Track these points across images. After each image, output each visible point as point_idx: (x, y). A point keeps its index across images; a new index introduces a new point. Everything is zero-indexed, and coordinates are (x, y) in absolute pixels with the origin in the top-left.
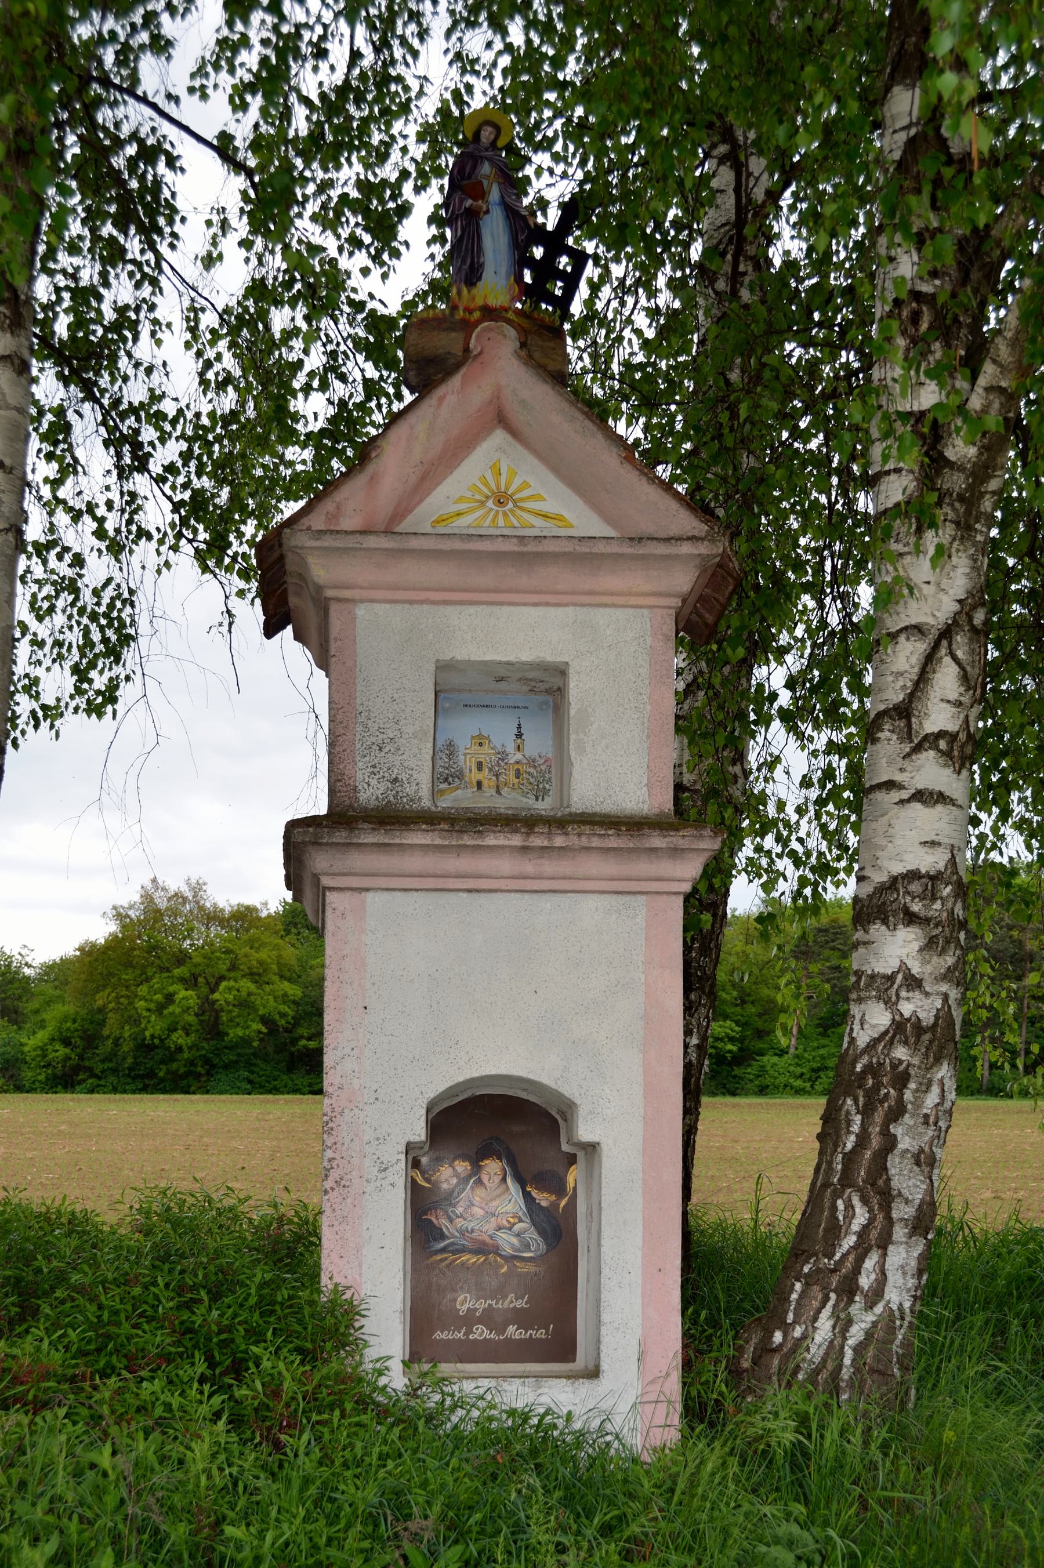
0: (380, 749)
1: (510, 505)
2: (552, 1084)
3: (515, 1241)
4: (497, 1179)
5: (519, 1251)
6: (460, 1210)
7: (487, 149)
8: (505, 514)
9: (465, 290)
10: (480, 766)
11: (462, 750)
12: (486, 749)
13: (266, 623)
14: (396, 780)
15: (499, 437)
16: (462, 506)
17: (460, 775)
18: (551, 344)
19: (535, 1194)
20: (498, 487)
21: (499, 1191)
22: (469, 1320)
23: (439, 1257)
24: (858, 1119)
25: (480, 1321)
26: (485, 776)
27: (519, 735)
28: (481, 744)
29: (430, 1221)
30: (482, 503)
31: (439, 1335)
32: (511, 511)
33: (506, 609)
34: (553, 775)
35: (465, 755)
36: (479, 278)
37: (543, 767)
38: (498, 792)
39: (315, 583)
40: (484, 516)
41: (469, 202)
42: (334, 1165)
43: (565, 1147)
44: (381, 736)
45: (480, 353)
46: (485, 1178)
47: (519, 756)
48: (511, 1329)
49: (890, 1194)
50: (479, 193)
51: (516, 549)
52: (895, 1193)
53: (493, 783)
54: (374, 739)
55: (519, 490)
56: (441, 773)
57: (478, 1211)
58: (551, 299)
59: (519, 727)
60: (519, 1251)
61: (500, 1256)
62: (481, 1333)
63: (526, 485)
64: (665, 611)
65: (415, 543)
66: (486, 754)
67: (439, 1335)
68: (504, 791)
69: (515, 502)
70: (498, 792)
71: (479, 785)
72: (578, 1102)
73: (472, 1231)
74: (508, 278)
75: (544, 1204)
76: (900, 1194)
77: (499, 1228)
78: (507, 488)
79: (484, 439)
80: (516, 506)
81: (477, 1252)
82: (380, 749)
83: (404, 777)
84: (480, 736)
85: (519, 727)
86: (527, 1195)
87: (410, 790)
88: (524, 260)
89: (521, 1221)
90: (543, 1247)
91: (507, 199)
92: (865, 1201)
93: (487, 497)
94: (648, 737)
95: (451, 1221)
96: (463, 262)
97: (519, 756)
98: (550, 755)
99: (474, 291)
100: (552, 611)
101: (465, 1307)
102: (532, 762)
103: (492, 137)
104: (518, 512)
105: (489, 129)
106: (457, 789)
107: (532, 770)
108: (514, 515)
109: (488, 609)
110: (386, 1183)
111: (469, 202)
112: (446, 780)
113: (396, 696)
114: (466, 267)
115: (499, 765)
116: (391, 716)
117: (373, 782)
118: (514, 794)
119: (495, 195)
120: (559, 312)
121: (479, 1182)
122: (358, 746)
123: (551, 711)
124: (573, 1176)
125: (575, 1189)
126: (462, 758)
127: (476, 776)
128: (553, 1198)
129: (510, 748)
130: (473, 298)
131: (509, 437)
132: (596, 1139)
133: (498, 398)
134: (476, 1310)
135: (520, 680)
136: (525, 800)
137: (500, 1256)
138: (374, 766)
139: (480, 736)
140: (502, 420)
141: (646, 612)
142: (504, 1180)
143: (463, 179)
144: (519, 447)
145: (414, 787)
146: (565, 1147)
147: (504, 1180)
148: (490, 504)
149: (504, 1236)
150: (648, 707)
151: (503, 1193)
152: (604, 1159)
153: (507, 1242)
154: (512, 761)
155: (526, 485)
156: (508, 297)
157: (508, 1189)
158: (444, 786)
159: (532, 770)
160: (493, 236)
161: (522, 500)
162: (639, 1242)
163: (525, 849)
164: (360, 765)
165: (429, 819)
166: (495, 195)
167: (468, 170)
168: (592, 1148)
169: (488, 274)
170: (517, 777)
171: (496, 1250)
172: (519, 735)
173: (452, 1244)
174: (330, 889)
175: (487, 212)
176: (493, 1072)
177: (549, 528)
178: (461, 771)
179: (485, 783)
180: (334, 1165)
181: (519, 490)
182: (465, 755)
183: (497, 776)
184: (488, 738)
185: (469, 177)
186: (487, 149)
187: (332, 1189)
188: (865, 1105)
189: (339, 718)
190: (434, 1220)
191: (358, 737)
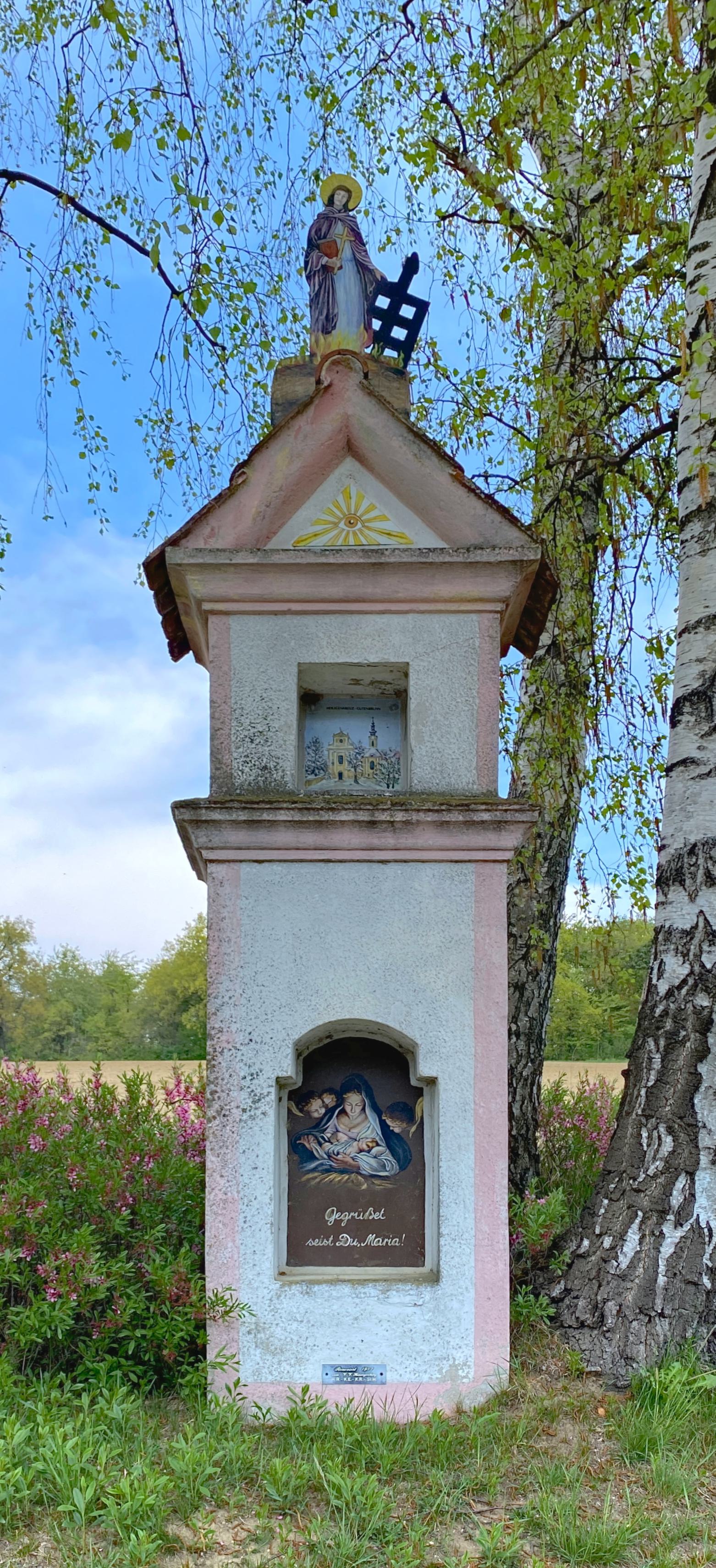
0: (252, 741)
1: (359, 525)
2: (398, 1028)
3: (373, 1162)
4: (358, 1109)
5: (376, 1170)
6: (327, 1135)
7: (340, 211)
8: (355, 533)
9: (321, 337)
10: (341, 760)
11: (326, 746)
12: (346, 745)
13: (170, 645)
14: (265, 768)
15: (349, 464)
16: (318, 528)
17: (324, 768)
18: (396, 384)
19: (389, 1122)
20: (349, 509)
21: (359, 1120)
22: (337, 1229)
23: (310, 1176)
24: (657, 1059)
25: (345, 1230)
26: (345, 767)
27: (373, 733)
28: (341, 741)
29: (304, 1146)
30: (336, 525)
31: (310, 1243)
32: (360, 530)
33: (356, 618)
34: (401, 767)
35: (328, 750)
36: (334, 327)
37: (393, 760)
38: (356, 781)
39: (195, 597)
40: (337, 536)
41: (325, 260)
42: (216, 1097)
43: (414, 1082)
44: (252, 730)
45: (329, 386)
46: (348, 1109)
47: (373, 751)
48: (371, 1237)
49: (697, 1126)
50: (333, 252)
51: (362, 561)
52: (700, 1124)
53: (352, 773)
54: (246, 733)
55: (367, 512)
56: (309, 767)
57: (342, 1137)
58: (395, 344)
59: (373, 726)
60: (376, 1170)
61: (361, 1174)
62: (346, 1240)
63: (372, 507)
64: (491, 615)
65: (276, 559)
66: (346, 750)
67: (310, 1243)
68: (361, 780)
69: (363, 522)
70: (356, 781)
71: (340, 775)
72: (419, 1042)
73: (338, 1154)
74: (358, 327)
75: (397, 1130)
76: (704, 1127)
77: (361, 1151)
78: (356, 510)
79: (337, 465)
80: (364, 526)
81: (342, 1172)
82: (252, 741)
83: (272, 765)
84: (341, 734)
85: (373, 726)
86: (384, 1126)
87: (277, 776)
88: (374, 312)
89: (378, 1145)
90: (396, 1167)
91: (358, 255)
92: (670, 1131)
93: (341, 519)
94: (477, 726)
95: (320, 1144)
96: (321, 313)
97: (373, 751)
98: (398, 749)
99: (330, 338)
100: (396, 619)
101: (332, 1219)
102: (384, 756)
103: (345, 200)
104: (367, 531)
105: (342, 193)
106: (322, 779)
107: (384, 762)
108: (362, 533)
109: (340, 618)
110: (258, 1112)
111: (325, 260)
112: (313, 772)
113: (264, 695)
114: (323, 317)
115: (357, 759)
116: (260, 712)
117: (247, 770)
118: (369, 783)
119: (346, 252)
120: (402, 355)
121: (343, 1112)
122: (233, 739)
123: (399, 710)
124: (423, 1106)
125: (422, 1118)
126: (326, 753)
127: (337, 768)
128: (404, 1125)
129: (366, 744)
130: (329, 345)
131: (357, 465)
132: (434, 1075)
133: (347, 427)
134: (341, 1221)
135: (372, 683)
136: (378, 788)
137: (361, 1174)
138: (247, 756)
139: (341, 734)
140: (351, 448)
141: (474, 617)
142: (364, 1109)
143: (319, 238)
144: (363, 470)
145: (280, 774)
146: (414, 1082)
147: (364, 1109)
148: (342, 525)
149: (364, 1158)
150: (477, 701)
151: (363, 1121)
152: (441, 1092)
153: (366, 1163)
154: (367, 755)
155: (372, 507)
156: (359, 343)
157: (366, 1117)
158: (312, 777)
159: (384, 762)
160: (345, 288)
161: (369, 520)
162: (471, 1163)
163: (372, 824)
164: (235, 755)
165: (293, 801)
166: (346, 252)
167: (323, 231)
168: (432, 1082)
169: (342, 322)
170: (372, 768)
171: (357, 1170)
172: (373, 733)
173: (322, 1164)
174: (212, 861)
175: (341, 268)
176: (347, 1017)
177: (393, 543)
178: (325, 765)
179: (345, 774)
180: (216, 1097)
181: (367, 512)
182: (328, 750)
183: (355, 768)
184: (347, 735)
185: (325, 237)
186: (340, 211)
187: (214, 1118)
188: (667, 1047)
189: (217, 715)
190: (307, 1145)
191: (233, 731)
